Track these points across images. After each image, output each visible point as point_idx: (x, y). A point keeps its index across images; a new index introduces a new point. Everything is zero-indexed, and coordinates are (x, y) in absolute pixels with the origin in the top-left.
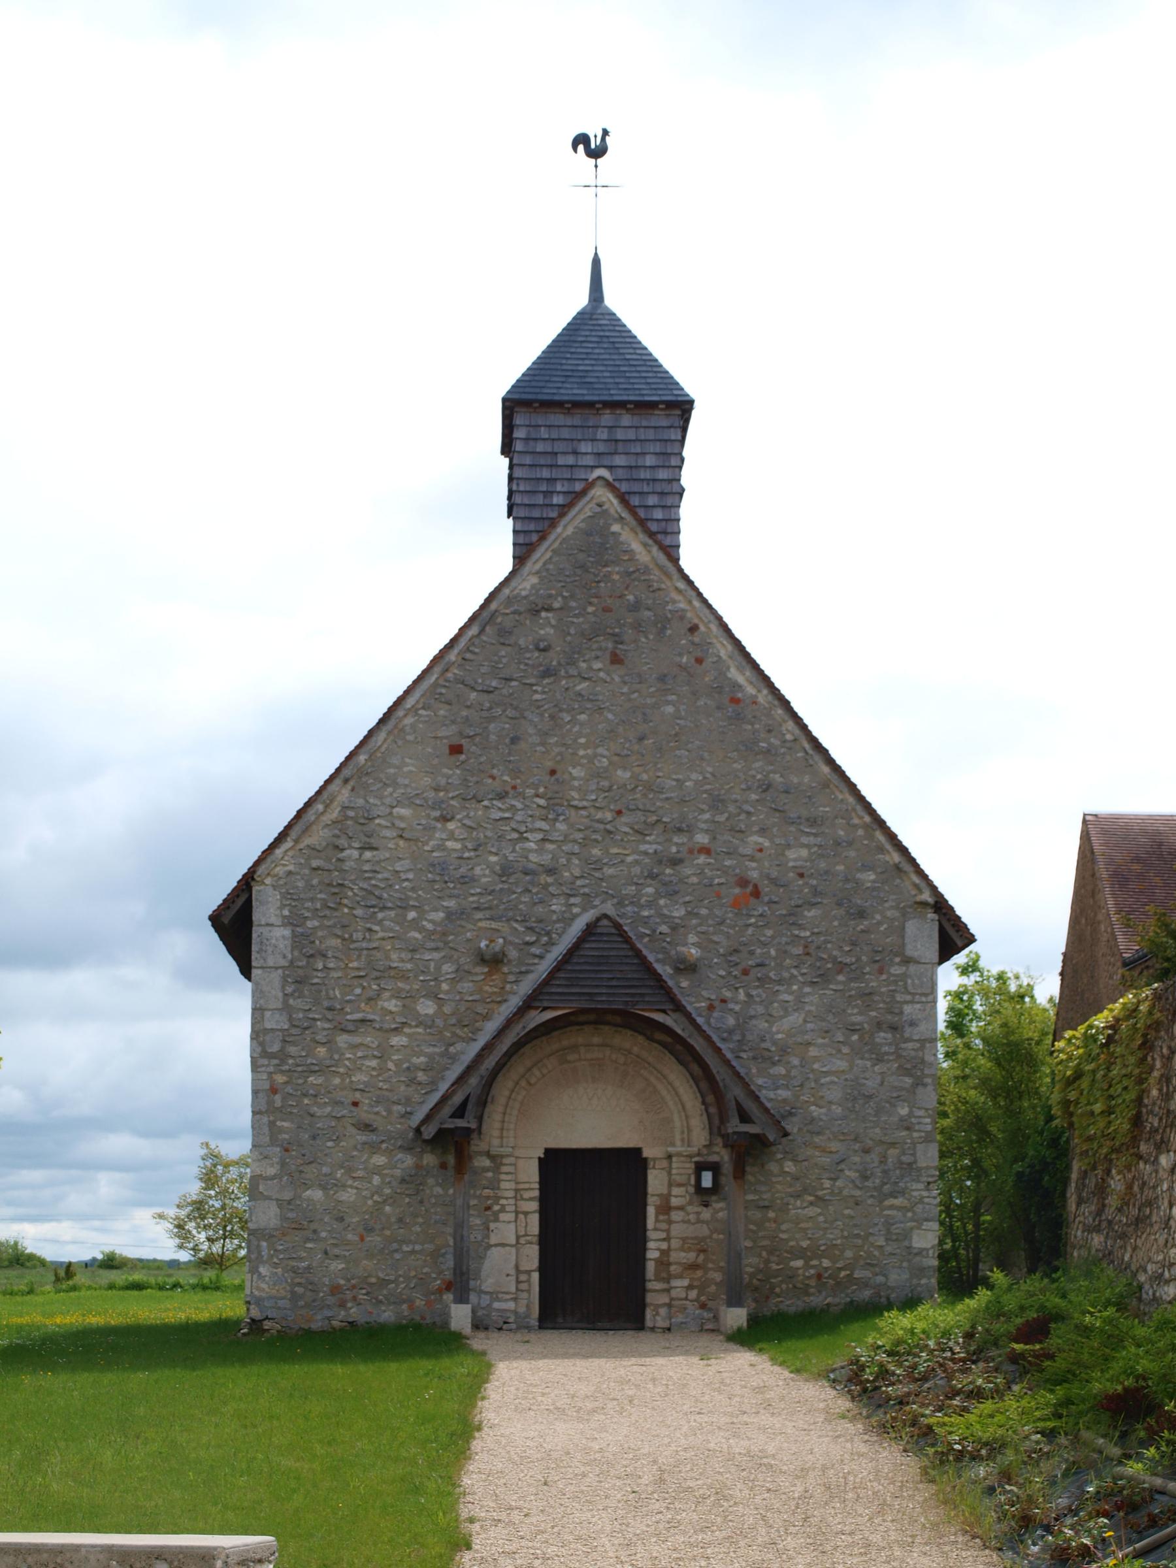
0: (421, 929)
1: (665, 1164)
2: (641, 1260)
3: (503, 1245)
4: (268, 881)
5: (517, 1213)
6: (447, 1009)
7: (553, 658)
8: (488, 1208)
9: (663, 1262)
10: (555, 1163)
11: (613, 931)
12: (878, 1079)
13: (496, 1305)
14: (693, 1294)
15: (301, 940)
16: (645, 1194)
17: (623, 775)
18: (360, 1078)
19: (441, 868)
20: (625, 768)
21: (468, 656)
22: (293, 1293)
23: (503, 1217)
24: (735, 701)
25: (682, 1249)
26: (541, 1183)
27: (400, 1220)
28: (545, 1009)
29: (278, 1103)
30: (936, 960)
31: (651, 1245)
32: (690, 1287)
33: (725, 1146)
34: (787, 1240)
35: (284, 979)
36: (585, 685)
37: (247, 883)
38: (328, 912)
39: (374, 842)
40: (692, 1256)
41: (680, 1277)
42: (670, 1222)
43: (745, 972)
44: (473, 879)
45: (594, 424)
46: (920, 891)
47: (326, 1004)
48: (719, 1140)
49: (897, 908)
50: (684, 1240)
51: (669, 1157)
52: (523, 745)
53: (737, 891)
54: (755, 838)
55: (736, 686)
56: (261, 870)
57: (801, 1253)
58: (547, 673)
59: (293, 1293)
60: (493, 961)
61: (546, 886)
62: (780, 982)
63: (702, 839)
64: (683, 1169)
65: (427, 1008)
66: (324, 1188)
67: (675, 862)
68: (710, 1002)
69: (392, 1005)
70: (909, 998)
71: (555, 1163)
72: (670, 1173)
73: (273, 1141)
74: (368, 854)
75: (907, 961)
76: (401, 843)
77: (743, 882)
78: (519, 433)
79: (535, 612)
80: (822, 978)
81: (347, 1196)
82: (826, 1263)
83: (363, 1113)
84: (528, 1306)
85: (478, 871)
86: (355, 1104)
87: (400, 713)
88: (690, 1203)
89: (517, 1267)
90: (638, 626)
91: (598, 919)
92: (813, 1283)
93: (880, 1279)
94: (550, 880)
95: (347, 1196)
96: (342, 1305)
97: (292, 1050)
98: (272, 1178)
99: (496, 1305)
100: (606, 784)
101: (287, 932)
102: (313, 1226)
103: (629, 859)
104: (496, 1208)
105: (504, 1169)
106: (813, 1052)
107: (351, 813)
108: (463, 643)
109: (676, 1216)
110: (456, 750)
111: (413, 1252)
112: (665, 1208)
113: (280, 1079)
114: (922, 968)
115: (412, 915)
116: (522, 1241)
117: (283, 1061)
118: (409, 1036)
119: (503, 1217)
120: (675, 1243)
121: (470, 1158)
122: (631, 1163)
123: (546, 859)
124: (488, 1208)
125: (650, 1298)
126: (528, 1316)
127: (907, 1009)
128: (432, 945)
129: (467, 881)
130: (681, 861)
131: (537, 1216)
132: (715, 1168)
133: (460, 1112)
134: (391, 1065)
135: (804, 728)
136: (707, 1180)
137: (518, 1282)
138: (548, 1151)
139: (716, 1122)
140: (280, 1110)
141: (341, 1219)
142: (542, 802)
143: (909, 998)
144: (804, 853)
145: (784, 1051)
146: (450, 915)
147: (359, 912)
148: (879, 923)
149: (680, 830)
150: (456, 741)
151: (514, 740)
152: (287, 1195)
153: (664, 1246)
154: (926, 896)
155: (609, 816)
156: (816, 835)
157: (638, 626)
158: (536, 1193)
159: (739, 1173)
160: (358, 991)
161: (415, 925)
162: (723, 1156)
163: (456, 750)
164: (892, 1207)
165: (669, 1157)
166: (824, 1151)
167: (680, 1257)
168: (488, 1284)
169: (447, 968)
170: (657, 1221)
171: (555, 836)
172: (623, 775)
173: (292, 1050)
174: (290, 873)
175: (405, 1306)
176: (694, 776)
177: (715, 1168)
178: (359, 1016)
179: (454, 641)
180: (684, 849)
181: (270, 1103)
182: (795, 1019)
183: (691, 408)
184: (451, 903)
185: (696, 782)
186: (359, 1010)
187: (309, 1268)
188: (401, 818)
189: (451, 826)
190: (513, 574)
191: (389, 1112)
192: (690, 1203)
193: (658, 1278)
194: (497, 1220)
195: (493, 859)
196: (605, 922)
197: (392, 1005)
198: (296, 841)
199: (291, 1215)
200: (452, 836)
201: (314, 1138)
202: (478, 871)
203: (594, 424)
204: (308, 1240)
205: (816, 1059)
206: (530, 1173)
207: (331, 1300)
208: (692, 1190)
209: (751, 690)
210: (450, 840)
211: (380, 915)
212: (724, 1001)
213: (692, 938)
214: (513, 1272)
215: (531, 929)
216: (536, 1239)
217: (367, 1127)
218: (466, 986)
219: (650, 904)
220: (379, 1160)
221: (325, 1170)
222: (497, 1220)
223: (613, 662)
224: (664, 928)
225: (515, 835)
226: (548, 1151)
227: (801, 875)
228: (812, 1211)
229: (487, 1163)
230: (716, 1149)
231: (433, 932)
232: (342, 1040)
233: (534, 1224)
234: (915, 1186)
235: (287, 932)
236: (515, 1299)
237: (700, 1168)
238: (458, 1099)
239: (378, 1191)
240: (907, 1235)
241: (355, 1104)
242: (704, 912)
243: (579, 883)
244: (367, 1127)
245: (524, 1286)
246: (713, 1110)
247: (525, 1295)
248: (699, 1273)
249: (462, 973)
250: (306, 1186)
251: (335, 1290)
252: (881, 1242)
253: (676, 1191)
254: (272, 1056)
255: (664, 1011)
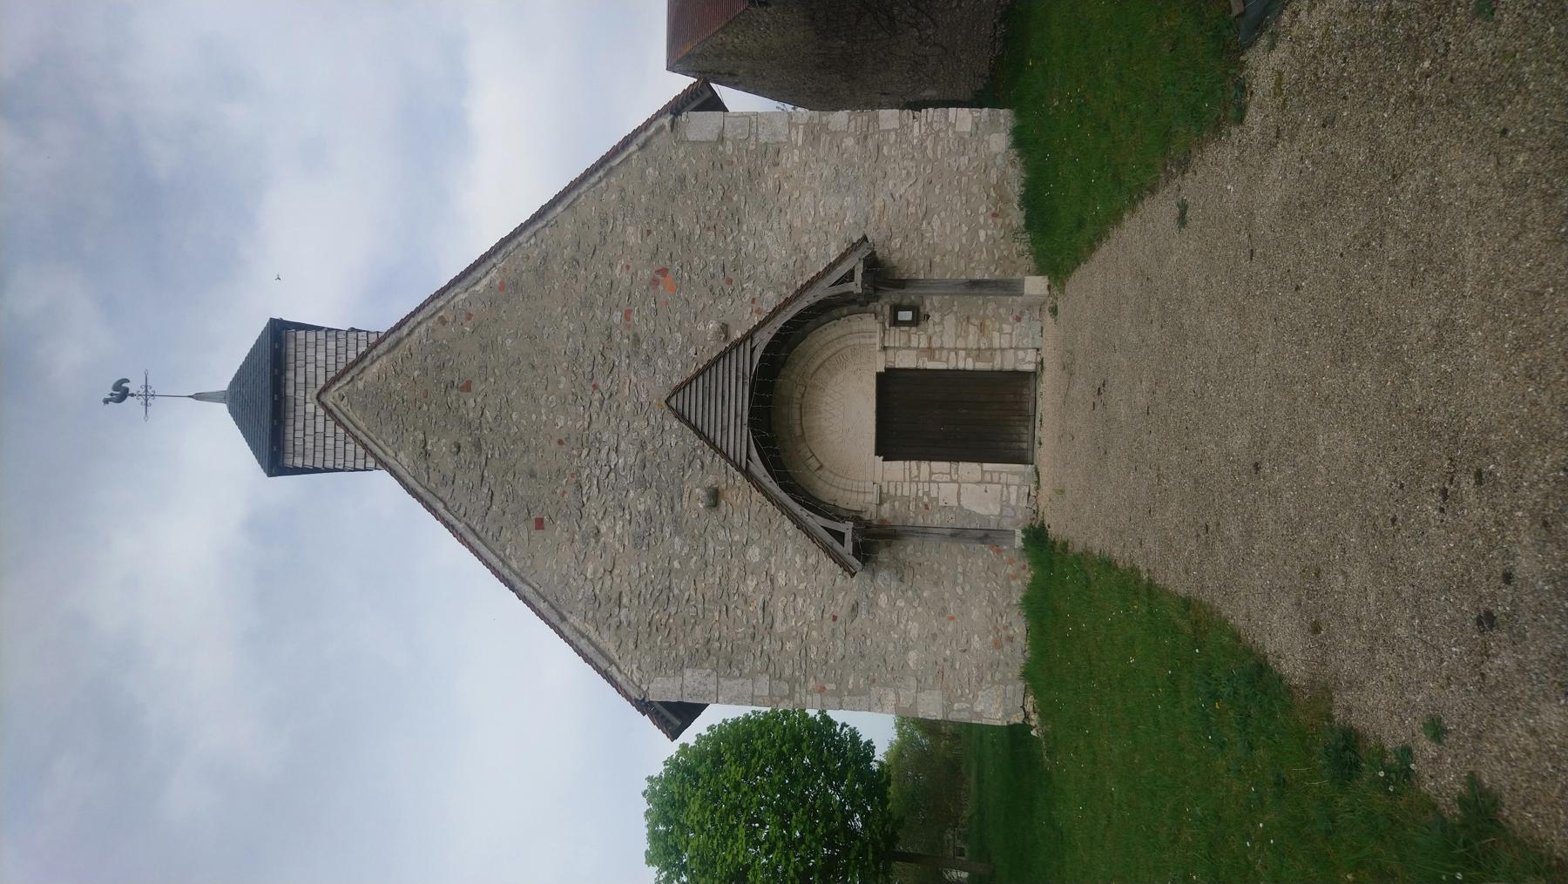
0: (689, 557)
1: (890, 352)
2: (974, 373)
3: (959, 494)
4: (644, 687)
5: (930, 481)
6: (756, 536)
7: (466, 441)
8: (926, 507)
9: (978, 353)
10: (890, 445)
11: (680, 395)
12: (822, 164)
13: (1013, 502)
14: (1007, 328)
15: (695, 660)
16: (917, 370)
17: (563, 384)
18: (811, 614)
19: (638, 540)
20: (559, 382)
21: (462, 511)
22: (1000, 682)
23: (934, 494)
24: (502, 287)
25: (966, 338)
26: (904, 459)
27: (936, 584)
28: (748, 457)
29: (832, 686)
30: (720, 114)
31: (961, 366)
32: (1000, 331)
33: (877, 299)
34: (961, 245)
35: (728, 677)
36: (488, 413)
37: (644, 706)
38: (672, 636)
39: (615, 596)
40: (972, 329)
41: (991, 340)
42: (942, 348)
43: (730, 281)
44: (648, 511)
45: (106, 401)
46: (662, 127)
47: (749, 640)
48: (871, 305)
49: (677, 149)
50: (958, 337)
51: (885, 348)
52: (537, 468)
53: (661, 288)
54: (617, 271)
55: (490, 286)
56: (634, 694)
57: (973, 233)
58: (478, 446)
59: (1000, 682)
60: (715, 497)
61: (656, 451)
62: (738, 251)
63: (617, 317)
64: (896, 337)
65: (754, 554)
66: (907, 649)
67: (637, 341)
68: (749, 309)
69: (751, 584)
70: (753, 138)
71: (890, 445)
72: (899, 348)
73: (866, 692)
74: (625, 600)
75: (721, 139)
76: (616, 572)
77: (655, 282)
78: (299, 462)
79: (427, 454)
80: (736, 217)
81: (914, 629)
82: (983, 209)
83: (843, 613)
84: (1014, 474)
85: (641, 508)
86: (835, 618)
87: (506, 572)
88: (925, 331)
89: (978, 483)
90: (441, 367)
91: (670, 408)
92: (999, 221)
93: (999, 160)
94: (650, 447)
95: (914, 629)
96: (1011, 639)
97: (788, 671)
98: (897, 694)
99: (1013, 502)
100: (570, 397)
101: (688, 673)
102: (941, 661)
103: (634, 379)
104: (926, 499)
105: (892, 491)
106: (797, 223)
107: (590, 615)
108: (449, 517)
109: (936, 343)
110: (540, 524)
111: (964, 574)
112: (930, 352)
113: (812, 684)
114: (728, 127)
115: (676, 564)
116: (955, 477)
117: (797, 680)
118: (777, 570)
119: (934, 494)
120: (961, 344)
121: (883, 521)
122: (888, 382)
123: (632, 450)
124: (926, 507)
125: (1008, 367)
126: (1022, 474)
127: (763, 139)
128: (702, 548)
129: (649, 517)
130: (635, 335)
131: (933, 464)
132: (896, 309)
133: (840, 536)
134: (802, 586)
135: (523, 227)
136: (906, 316)
137: (991, 482)
138: (878, 453)
139: (855, 307)
140: (839, 684)
141: (934, 636)
142: (585, 452)
143: (753, 138)
144: (630, 230)
145: (796, 249)
146: (677, 531)
147: (673, 610)
148: (690, 163)
149: (609, 336)
150: (532, 525)
151: (532, 475)
152: (913, 683)
153: (962, 353)
154: (666, 121)
155: (597, 396)
156: (615, 219)
157: (441, 367)
158: (914, 463)
159: (901, 284)
160: (739, 612)
161: (684, 562)
162: (884, 305)
163: (540, 524)
164: (934, 152)
165: (885, 348)
166: (882, 213)
167: (972, 340)
168: (993, 510)
169: (721, 534)
170: (939, 360)
171: (613, 441)
172: (563, 384)
173: (788, 671)
174: (639, 668)
175: (1013, 583)
176: (565, 323)
177: (896, 309)
178: (760, 612)
179: (447, 525)
180: (626, 333)
181: (833, 693)
182: (769, 238)
183: (281, 321)
184: (667, 531)
185: (570, 321)
186: (754, 613)
187: (977, 667)
188: (595, 572)
189: (603, 529)
190: (393, 473)
191: (842, 589)
192: (925, 331)
193: (992, 359)
194: (937, 499)
195: (632, 494)
196: (673, 402)
197: (751, 584)
198: (612, 662)
199: (930, 681)
200: (612, 529)
201: (863, 656)
202: (641, 508)
203: (106, 401)
204: (952, 666)
205: (804, 221)
206: (897, 468)
207: (1007, 648)
208: (914, 329)
209: (494, 273)
210: (615, 530)
211: (676, 591)
212: (753, 301)
213: (701, 327)
214: (983, 487)
215: (690, 463)
216: (954, 465)
217: (855, 609)
218: (737, 519)
219: (670, 362)
220: (883, 600)
221: (891, 647)
222: (937, 499)
223: (469, 390)
224: (692, 351)
225: (612, 475)
226: (878, 453)
227: (649, 232)
228: (936, 222)
229: (886, 506)
230: (879, 308)
231: (691, 547)
232: (779, 628)
233: (939, 466)
234: (916, 130)
235: (688, 673)
236: (1008, 486)
237: (896, 322)
238: (829, 538)
239: (909, 602)
240: (960, 137)
241: (835, 618)
242: (678, 317)
243: (653, 422)
244: (855, 609)
245: (996, 478)
246: (845, 311)
247: (1004, 476)
248: (988, 323)
249: (726, 523)
250: (905, 666)
251: (997, 645)
252: (964, 160)
253: (914, 344)
254: (792, 690)
255: (752, 350)
